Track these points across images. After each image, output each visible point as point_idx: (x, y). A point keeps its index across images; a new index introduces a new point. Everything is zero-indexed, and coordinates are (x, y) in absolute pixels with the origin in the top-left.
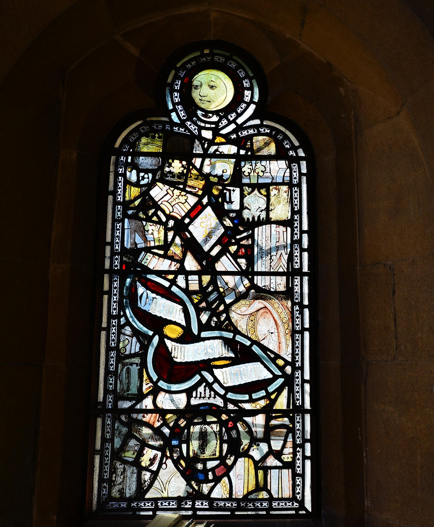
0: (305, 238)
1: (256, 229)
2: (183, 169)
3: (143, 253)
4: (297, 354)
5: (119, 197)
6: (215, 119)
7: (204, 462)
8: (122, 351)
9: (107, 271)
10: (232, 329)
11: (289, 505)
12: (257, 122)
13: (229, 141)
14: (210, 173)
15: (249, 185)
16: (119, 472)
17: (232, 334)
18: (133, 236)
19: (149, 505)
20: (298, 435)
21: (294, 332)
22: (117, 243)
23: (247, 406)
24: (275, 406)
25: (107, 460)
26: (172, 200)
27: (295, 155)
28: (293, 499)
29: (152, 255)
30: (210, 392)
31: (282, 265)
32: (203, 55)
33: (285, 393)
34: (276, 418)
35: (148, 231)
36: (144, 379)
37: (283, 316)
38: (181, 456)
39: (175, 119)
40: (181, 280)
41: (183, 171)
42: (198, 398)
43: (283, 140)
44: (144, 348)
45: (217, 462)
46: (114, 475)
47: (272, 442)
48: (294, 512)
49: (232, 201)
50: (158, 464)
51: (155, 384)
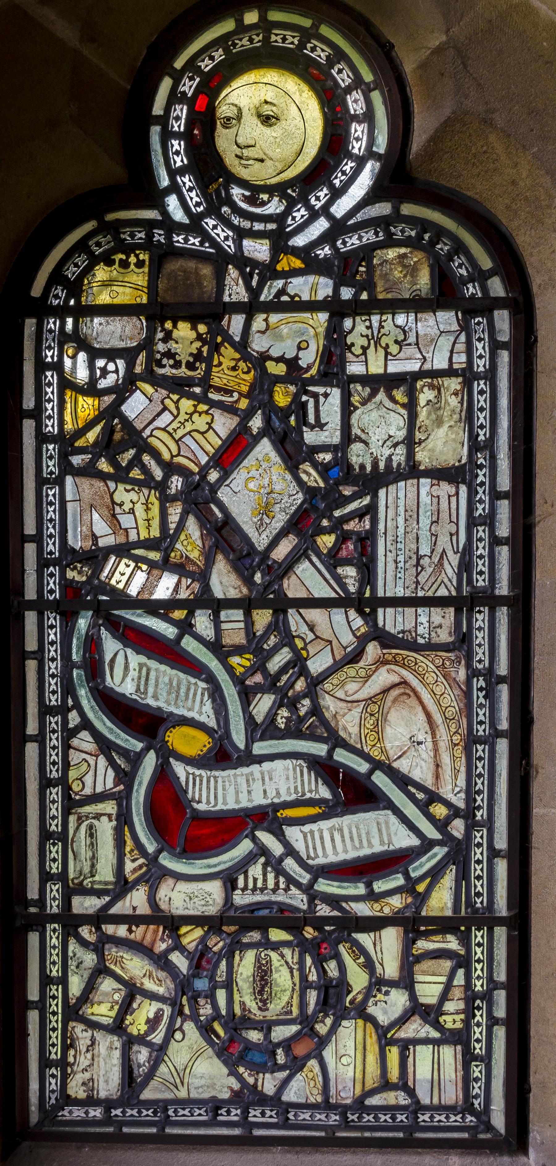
0: (504, 508)
4: (479, 792)
7: (266, 1027)
10: (325, 735)
11: (455, 1119)
12: (383, 209)
13: (312, 265)
14: (268, 351)
15: (366, 380)
18: (86, 517)
19: (147, 1113)
21: (471, 741)
23: (362, 909)
24: (425, 908)
25: (55, 1021)
26: (175, 425)
28: (468, 1107)
30: (276, 877)
31: (446, 580)
32: (242, 28)
33: (448, 880)
34: (426, 935)
35: (121, 505)
36: (128, 849)
37: (445, 703)
38: (217, 1016)
39: (178, 215)
40: (202, 622)
41: (199, 350)
42: (249, 892)
44: (126, 778)
45: (294, 1028)
46: (72, 1052)
49: (323, 421)
50: (164, 1030)
51: (153, 860)
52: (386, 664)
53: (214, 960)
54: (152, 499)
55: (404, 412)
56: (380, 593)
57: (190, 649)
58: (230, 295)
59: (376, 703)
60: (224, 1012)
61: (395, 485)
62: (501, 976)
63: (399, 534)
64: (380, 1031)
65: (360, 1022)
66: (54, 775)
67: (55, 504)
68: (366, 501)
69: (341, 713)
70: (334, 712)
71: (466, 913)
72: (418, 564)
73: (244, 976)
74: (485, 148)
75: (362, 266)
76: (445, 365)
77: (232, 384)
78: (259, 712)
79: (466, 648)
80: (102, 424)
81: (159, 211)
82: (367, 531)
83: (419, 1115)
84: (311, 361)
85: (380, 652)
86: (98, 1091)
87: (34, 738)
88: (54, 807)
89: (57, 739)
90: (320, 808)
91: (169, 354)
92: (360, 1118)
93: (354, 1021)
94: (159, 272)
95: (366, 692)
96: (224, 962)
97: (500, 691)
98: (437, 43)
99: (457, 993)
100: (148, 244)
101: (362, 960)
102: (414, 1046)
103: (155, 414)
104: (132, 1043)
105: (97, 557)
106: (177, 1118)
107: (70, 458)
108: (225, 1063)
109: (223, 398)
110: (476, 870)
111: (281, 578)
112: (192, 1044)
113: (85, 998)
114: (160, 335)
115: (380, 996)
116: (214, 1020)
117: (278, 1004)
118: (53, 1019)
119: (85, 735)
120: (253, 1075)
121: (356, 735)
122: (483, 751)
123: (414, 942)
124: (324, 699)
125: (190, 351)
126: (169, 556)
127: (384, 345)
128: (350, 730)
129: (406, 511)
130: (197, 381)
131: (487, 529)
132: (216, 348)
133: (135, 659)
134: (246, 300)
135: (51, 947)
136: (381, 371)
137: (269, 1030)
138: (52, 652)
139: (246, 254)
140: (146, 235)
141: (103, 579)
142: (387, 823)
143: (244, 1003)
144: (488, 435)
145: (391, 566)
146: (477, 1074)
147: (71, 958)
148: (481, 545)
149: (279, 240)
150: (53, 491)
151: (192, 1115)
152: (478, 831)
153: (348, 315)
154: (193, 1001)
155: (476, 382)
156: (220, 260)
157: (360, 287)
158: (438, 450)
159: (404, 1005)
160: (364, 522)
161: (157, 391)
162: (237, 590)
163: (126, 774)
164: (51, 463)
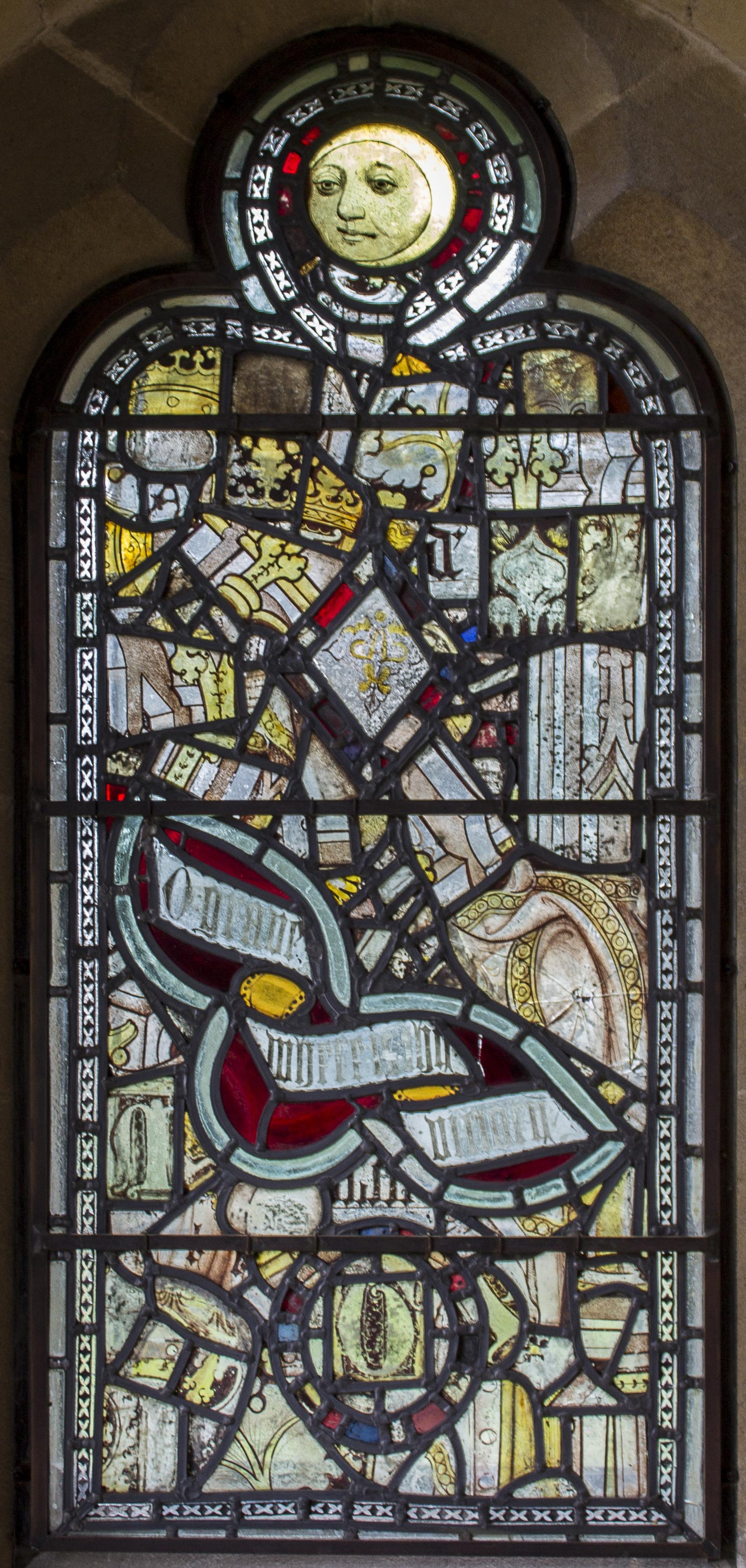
0: (695, 684)
1: (534, 662)
2: (290, 467)
3: (170, 745)
4: (666, 1067)
5: (86, 566)
6: (390, 294)
7: (377, 1391)
8: (118, 1061)
9: (58, 809)
10: (459, 987)
11: (637, 1517)
12: (535, 301)
13: (439, 368)
14: (381, 478)
15: (513, 517)
16: (124, 1416)
17: (459, 1004)
18: (135, 690)
19: (213, 1512)
20: (667, 1315)
21: (654, 996)
22: (86, 715)
23: (509, 1228)
24: (594, 1227)
25: (86, 1385)
26: (255, 570)
27: (662, 411)
28: (653, 1501)
29: (197, 754)
30: (393, 1184)
31: (619, 779)
32: (345, 76)
33: (626, 1187)
34: (597, 1263)
35: (182, 674)
36: (188, 1145)
37: (621, 943)
38: (310, 1376)
39: (259, 301)
40: (293, 833)
41: (289, 476)
42: (355, 1204)
43: (623, 363)
44: (186, 1046)
45: (417, 1393)
46: (109, 1428)
47: (586, 1337)
48: (652, 1539)
49: (455, 569)
50: (237, 1397)
51: (223, 1160)
52: (540, 891)
53: (307, 1299)
54: (225, 667)
55: (563, 558)
56: (532, 796)
57: (275, 869)
58: (330, 406)
59: (526, 943)
60: (320, 1372)
61: (551, 652)
62: (697, 1320)
63: (556, 717)
64: (534, 1396)
65: (508, 1384)
66: (89, 1042)
67: (92, 672)
68: (513, 672)
69: (481, 957)
70: (471, 956)
71: (649, 1232)
72: (582, 757)
73: (348, 1321)
74: (670, 232)
75: (507, 372)
76: (616, 499)
77: (333, 519)
78: (369, 955)
79: (646, 870)
80: (157, 568)
81: (234, 297)
82: (514, 713)
83: (588, 1512)
84: (439, 491)
85: (532, 874)
86: (145, 1481)
87: (61, 991)
88: (87, 1087)
89: (93, 993)
90: (452, 1088)
91: (248, 480)
92: (507, 1516)
93: (499, 1383)
94: (235, 368)
95: (514, 928)
96: (320, 1303)
97: (691, 929)
98: (608, 104)
99: (638, 1344)
100: (220, 339)
101: (509, 1298)
102: (581, 1418)
103: (228, 555)
104: (193, 1415)
105: (149, 744)
106: (254, 1518)
107: (113, 611)
108: (322, 1441)
109: (321, 537)
110: (663, 1173)
111: (399, 773)
112: (275, 1417)
113: (128, 1353)
114: (235, 455)
115: (534, 1349)
116: (306, 1381)
117: (395, 1361)
118: (85, 1382)
119: (130, 986)
120: (359, 1458)
121: (500, 987)
122: (671, 1010)
123: (579, 1274)
124: (456, 937)
125: (276, 475)
126: (247, 743)
127: (536, 473)
128: (493, 980)
129: (566, 686)
130: (285, 514)
131: (673, 712)
132: (311, 473)
133: (200, 881)
134: (352, 412)
135: (82, 1282)
136: (532, 505)
137: (382, 1396)
138: (87, 872)
139: (352, 353)
140: (216, 326)
141: (157, 773)
142: (542, 1109)
143: (347, 1358)
144: (673, 590)
145: (546, 759)
146: (666, 1455)
147: (110, 1298)
148: (665, 733)
149: (396, 337)
150: (91, 654)
151: (276, 1513)
152: (664, 1120)
153: (489, 434)
154: (277, 1356)
155: (657, 521)
156: (317, 361)
157: (505, 398)
158: (608, 608)
159: (567, 1361)
160: (510, 701)
161: (230, 526)
162: (340, 790)
163: (187, 1041)
164: (87, 618)
